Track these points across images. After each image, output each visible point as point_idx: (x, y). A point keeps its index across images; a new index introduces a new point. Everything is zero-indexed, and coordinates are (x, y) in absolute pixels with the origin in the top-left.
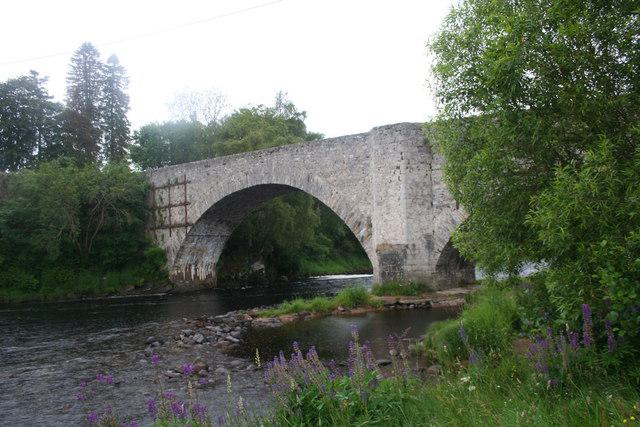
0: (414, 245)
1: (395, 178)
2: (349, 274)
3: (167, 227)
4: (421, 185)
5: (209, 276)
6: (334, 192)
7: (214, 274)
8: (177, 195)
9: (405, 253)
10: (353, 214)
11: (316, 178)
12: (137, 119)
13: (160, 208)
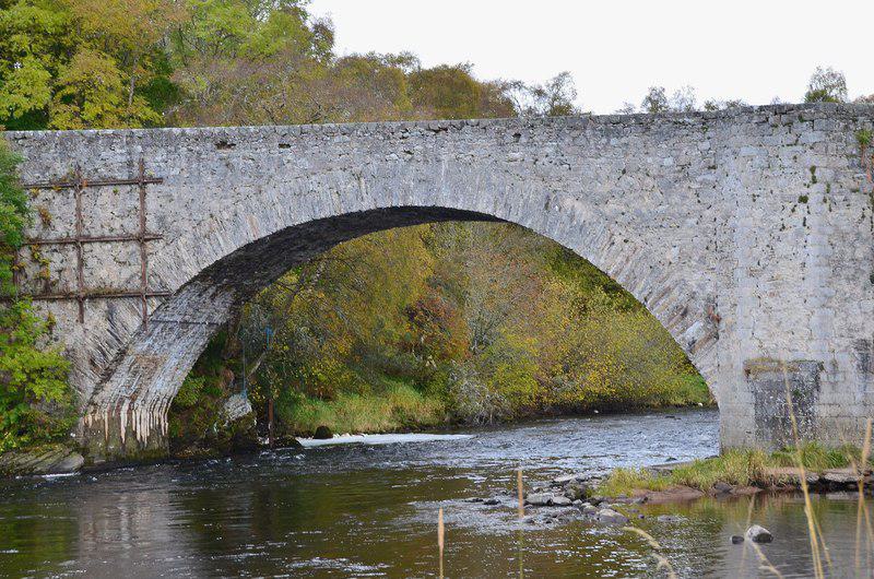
0: (834, 364)
1: (797, 220)
2: (360, 445)
3: (67, 297)
4: (852, 237)
5: (156, 430)
6: (618, 239)
7: (165, 425)
8: (107, 210)
9: (817, 379)
10: (667, 291)
11: (568, 202)
12: (341, 49)
13: (37, 243)
